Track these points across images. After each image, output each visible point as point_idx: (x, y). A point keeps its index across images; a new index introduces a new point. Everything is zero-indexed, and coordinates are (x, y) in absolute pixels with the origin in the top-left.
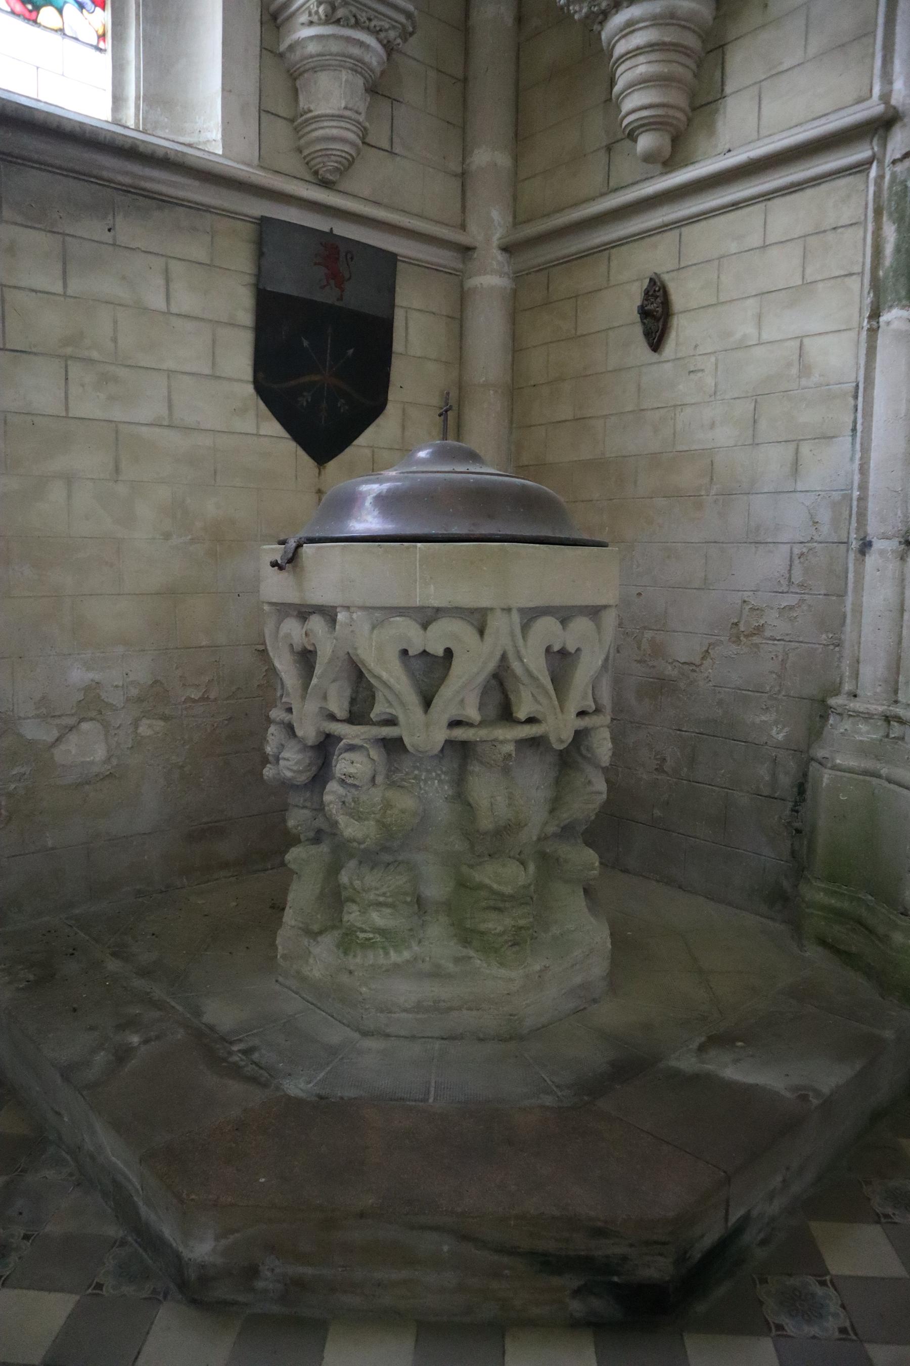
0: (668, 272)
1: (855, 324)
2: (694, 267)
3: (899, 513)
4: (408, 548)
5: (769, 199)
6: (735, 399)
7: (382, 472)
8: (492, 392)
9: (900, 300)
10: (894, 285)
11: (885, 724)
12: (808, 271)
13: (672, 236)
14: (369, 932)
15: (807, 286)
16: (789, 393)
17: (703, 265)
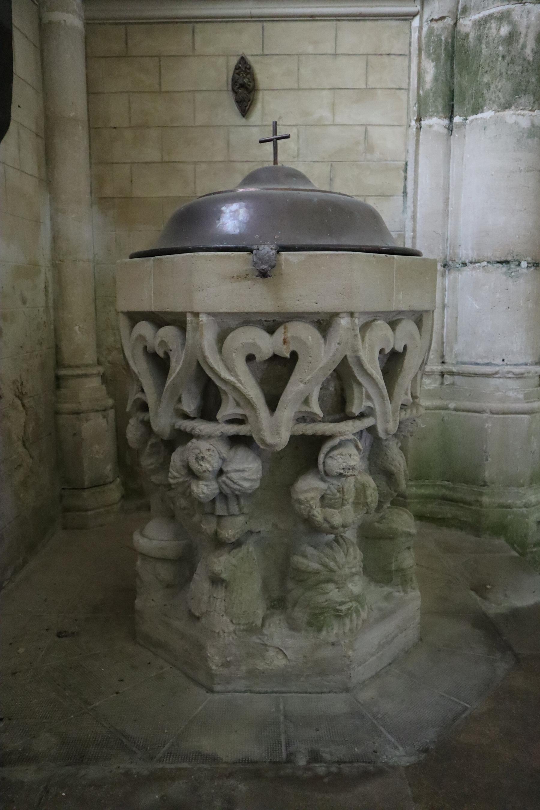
0: (252, 55)
1: (404, 121)
2: (276, 57)
3: (441, 248)
4: (390, 259)
5: (339, 20)
6: (314, 162)
7: (239, 190)
8: (80, 127)
9: (438, 112)
10: (434, 102)
11: (440, 377)
12: (371, 79)
13: (255, 27)
14: (348, 602)
15: (369, 90)
16: (357, 162)
17: (285, 56)
